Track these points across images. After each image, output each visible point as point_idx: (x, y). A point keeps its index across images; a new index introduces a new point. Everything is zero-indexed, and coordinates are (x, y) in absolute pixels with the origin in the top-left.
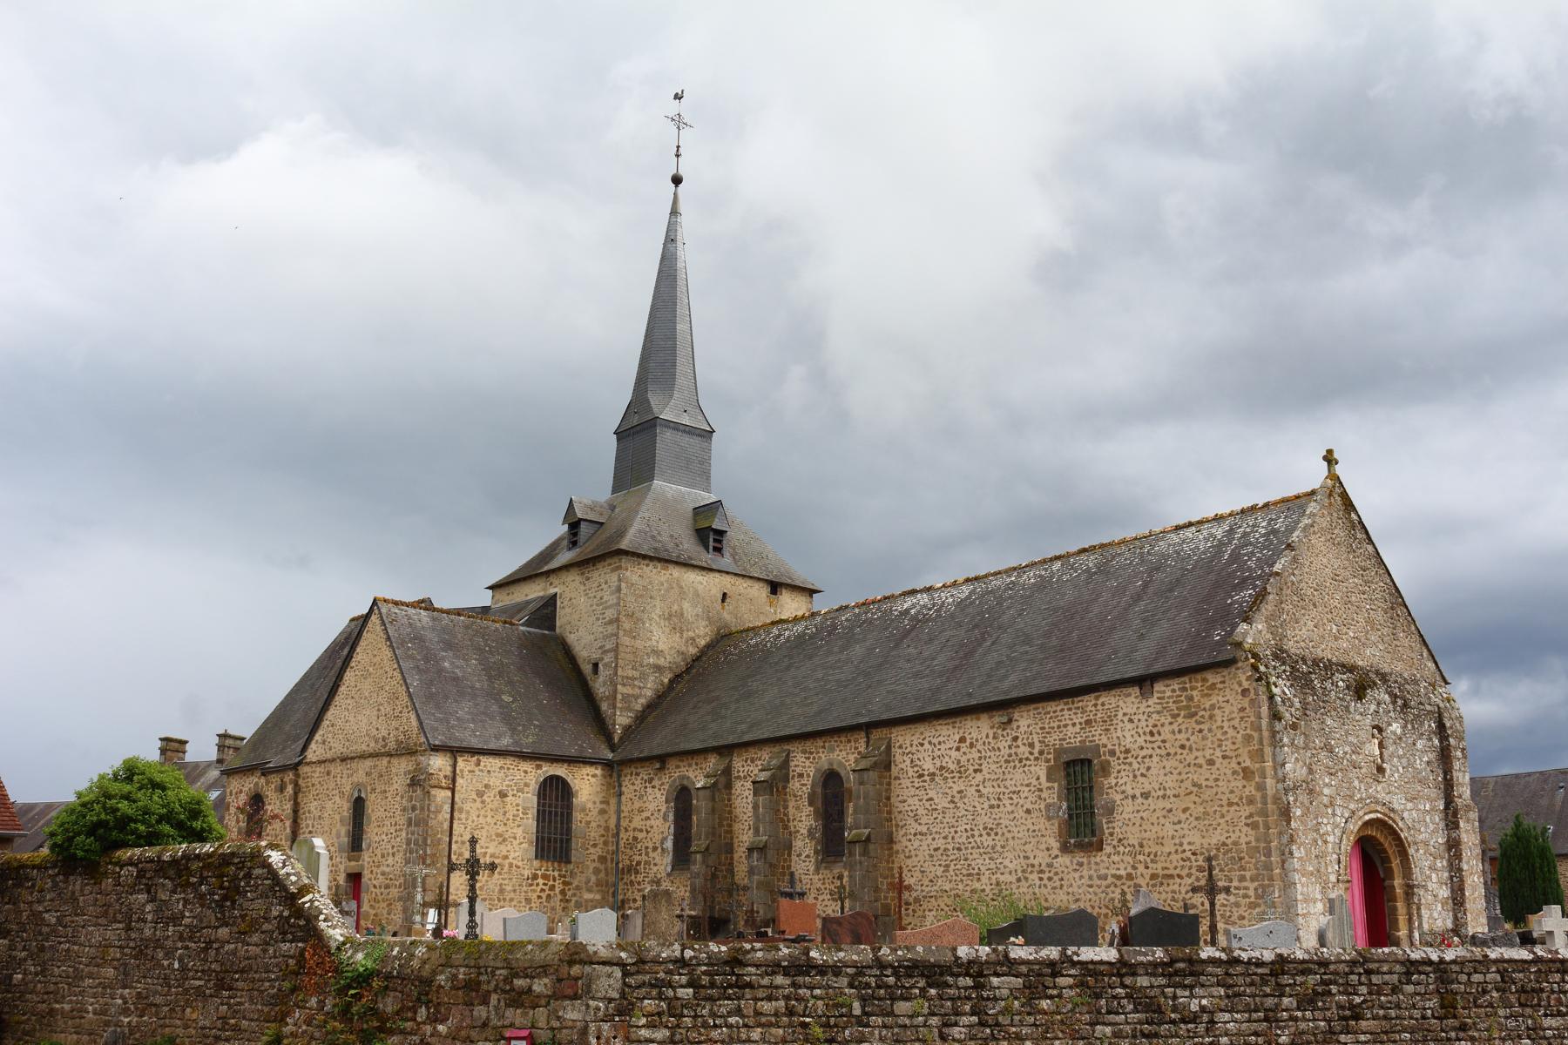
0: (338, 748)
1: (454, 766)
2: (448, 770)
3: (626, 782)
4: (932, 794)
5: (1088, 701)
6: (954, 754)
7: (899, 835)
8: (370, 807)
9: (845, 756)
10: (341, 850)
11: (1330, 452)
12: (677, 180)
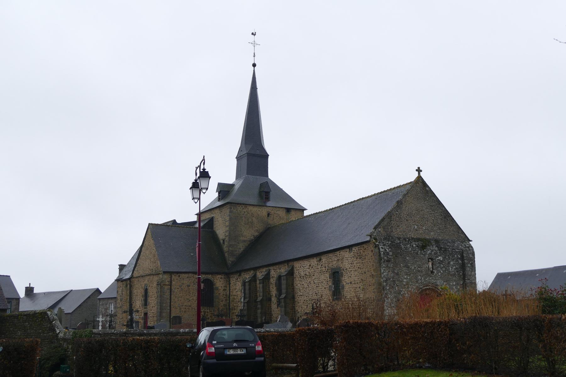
0: (141, 273)
1: (171, 278)
2: (169, 280)
3: (233, 280)
4: (303, 283)
5: (338, 253)
6: (308, 270)
7: (296, 297)
8: (149, 291)
9: (283, 270)
10: (142, 305)
11: (419, 168)
12: (254, 65)
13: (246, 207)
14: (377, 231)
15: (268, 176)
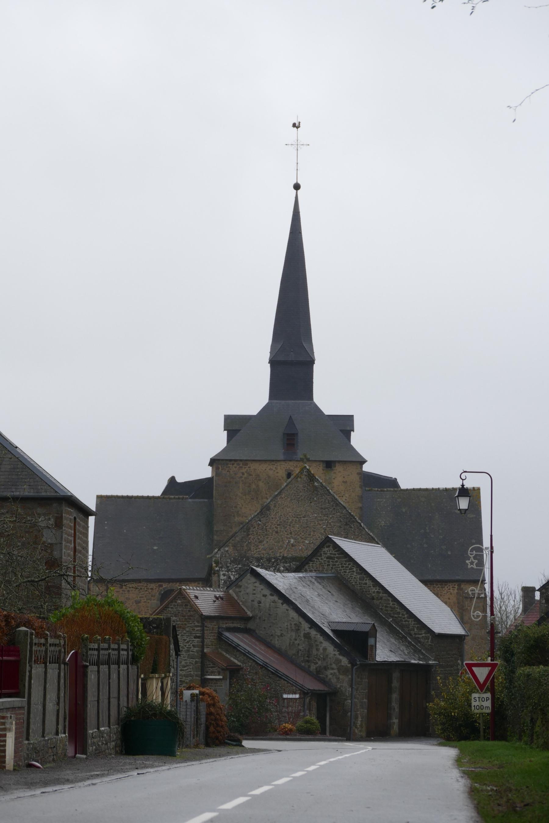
12: (297, 187)
13: (247, 464)
14: (222, 550)
15: (311, 397)
